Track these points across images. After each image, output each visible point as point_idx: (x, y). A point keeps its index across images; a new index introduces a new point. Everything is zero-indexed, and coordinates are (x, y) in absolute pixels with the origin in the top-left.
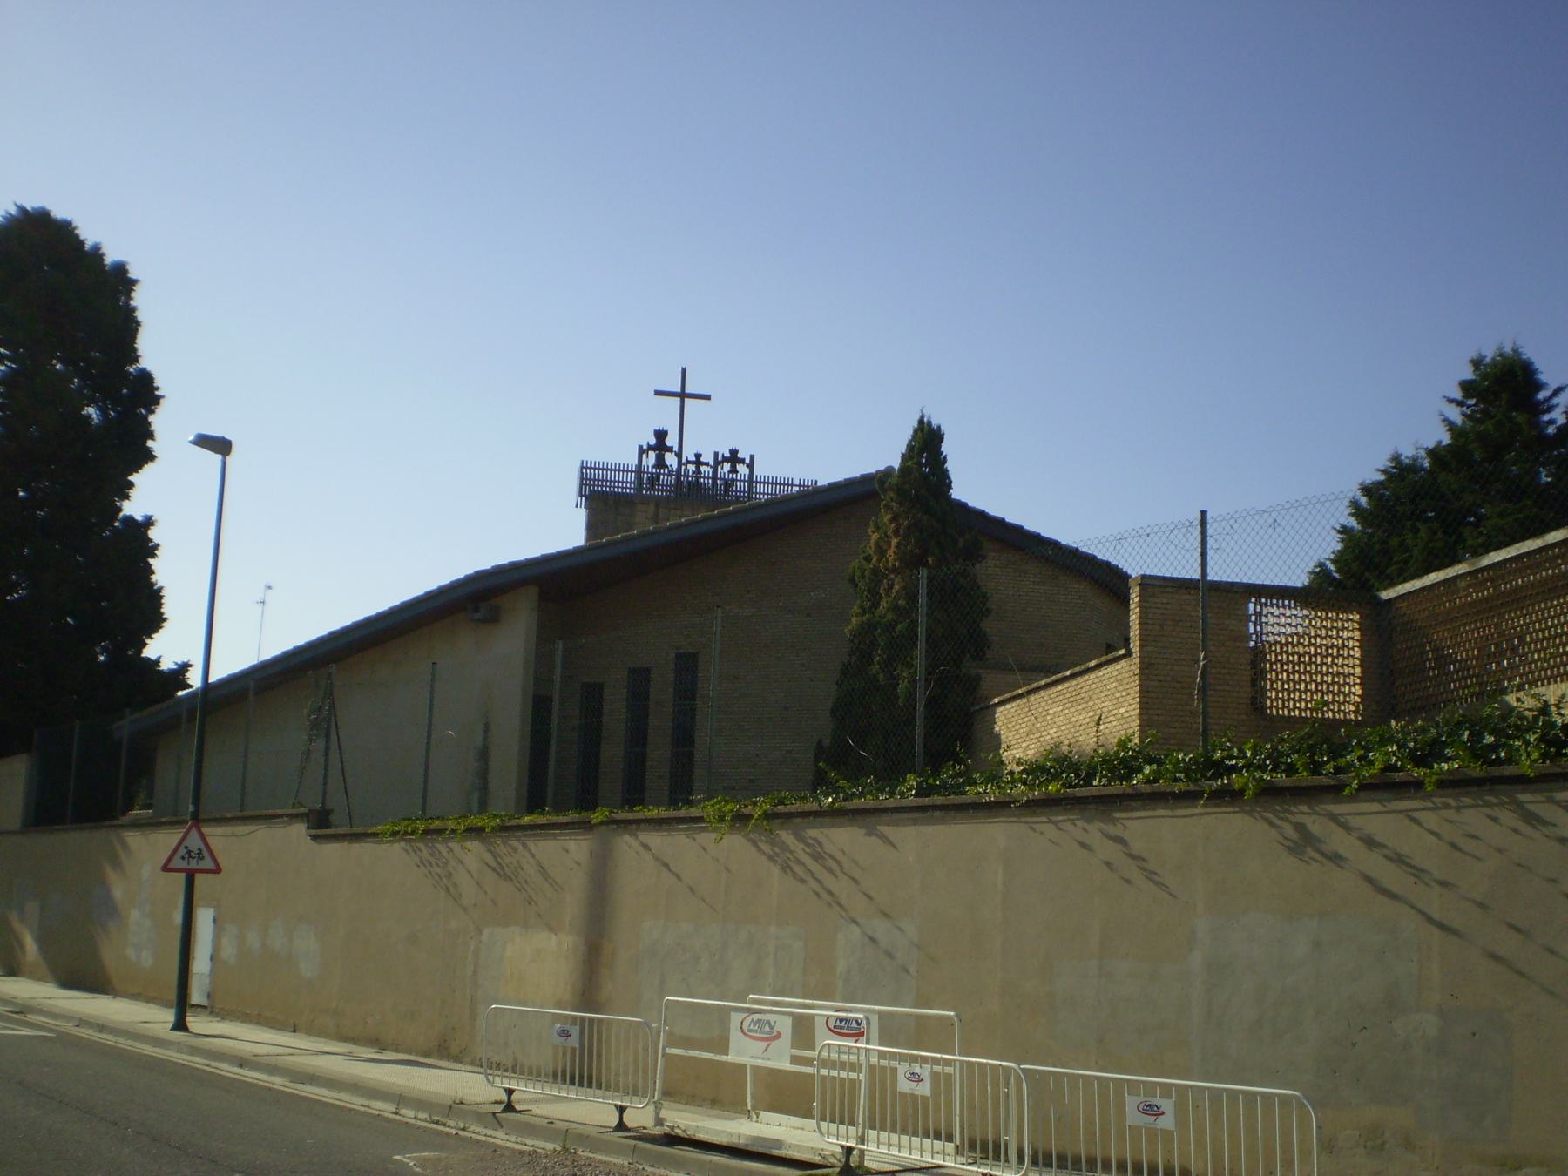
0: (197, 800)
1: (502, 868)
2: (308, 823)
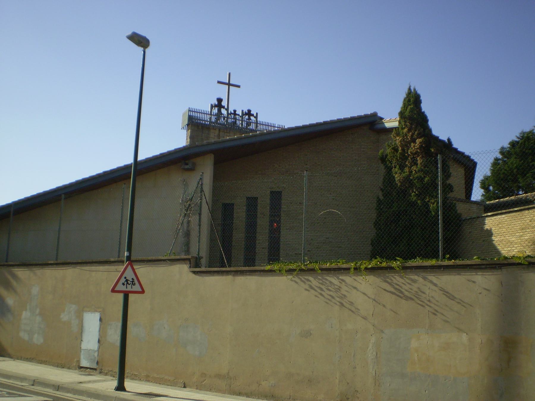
0: (129, 250)
1: (401, 292)
2: (190, 264)
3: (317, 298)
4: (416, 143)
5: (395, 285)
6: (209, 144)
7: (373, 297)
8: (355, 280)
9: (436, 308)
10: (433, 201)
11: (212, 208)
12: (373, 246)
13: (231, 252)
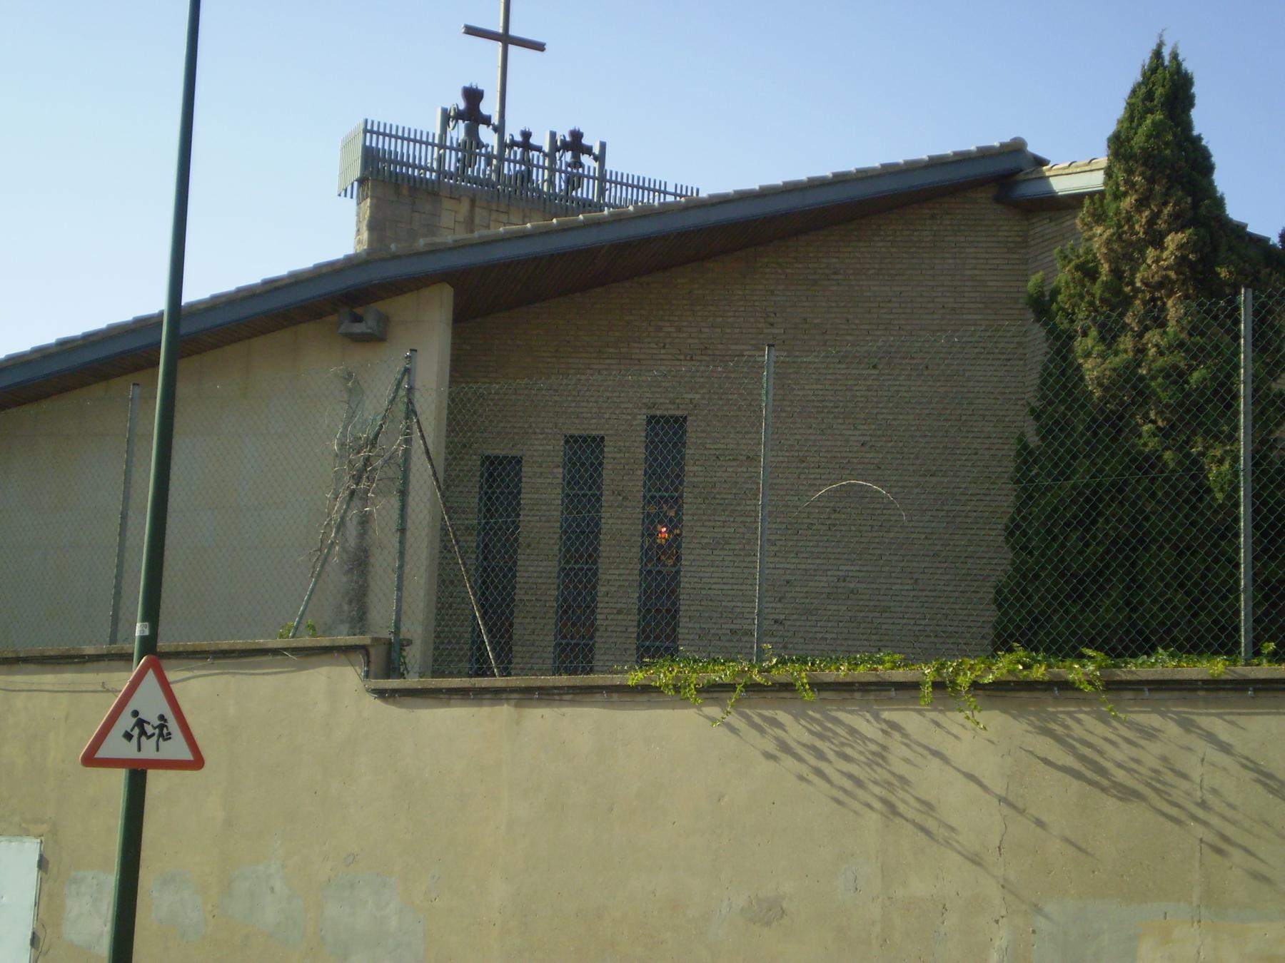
0: (152, 613)
1: (1102, 771)
2: (368, 663)
3: (804, 785)
4: (1167, 249)
5: (1078, 745)
6: (434, 251)
7: (1003, 793)
8: (938, 724)
9: (1229, 830)
10: (1218, 453)
11: (446, 470)
12: (1000, 606)
13: (511, 625)
